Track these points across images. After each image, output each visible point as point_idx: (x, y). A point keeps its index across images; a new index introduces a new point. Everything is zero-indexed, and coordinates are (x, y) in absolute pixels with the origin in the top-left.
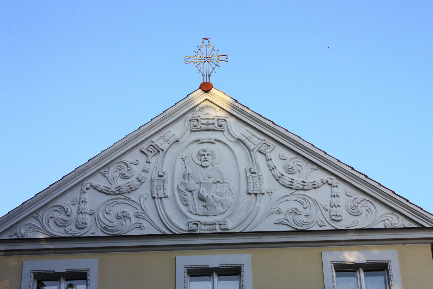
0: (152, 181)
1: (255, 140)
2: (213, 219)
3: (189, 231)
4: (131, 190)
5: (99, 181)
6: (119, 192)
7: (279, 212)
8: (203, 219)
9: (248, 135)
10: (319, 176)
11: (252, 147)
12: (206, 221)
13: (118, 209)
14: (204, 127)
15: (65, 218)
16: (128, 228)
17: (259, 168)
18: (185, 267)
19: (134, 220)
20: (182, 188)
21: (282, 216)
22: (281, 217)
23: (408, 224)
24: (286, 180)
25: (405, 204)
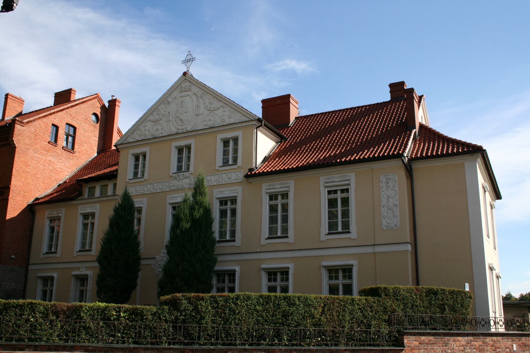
4: (160, 119)
5: (151, 118)
6: (157, 121)
10: (220, 104)
16: (158, 134)
18: (222, 140)
19: (160, 131)
21: (205, 123)
22: (205, 123)
23: (247, 119)
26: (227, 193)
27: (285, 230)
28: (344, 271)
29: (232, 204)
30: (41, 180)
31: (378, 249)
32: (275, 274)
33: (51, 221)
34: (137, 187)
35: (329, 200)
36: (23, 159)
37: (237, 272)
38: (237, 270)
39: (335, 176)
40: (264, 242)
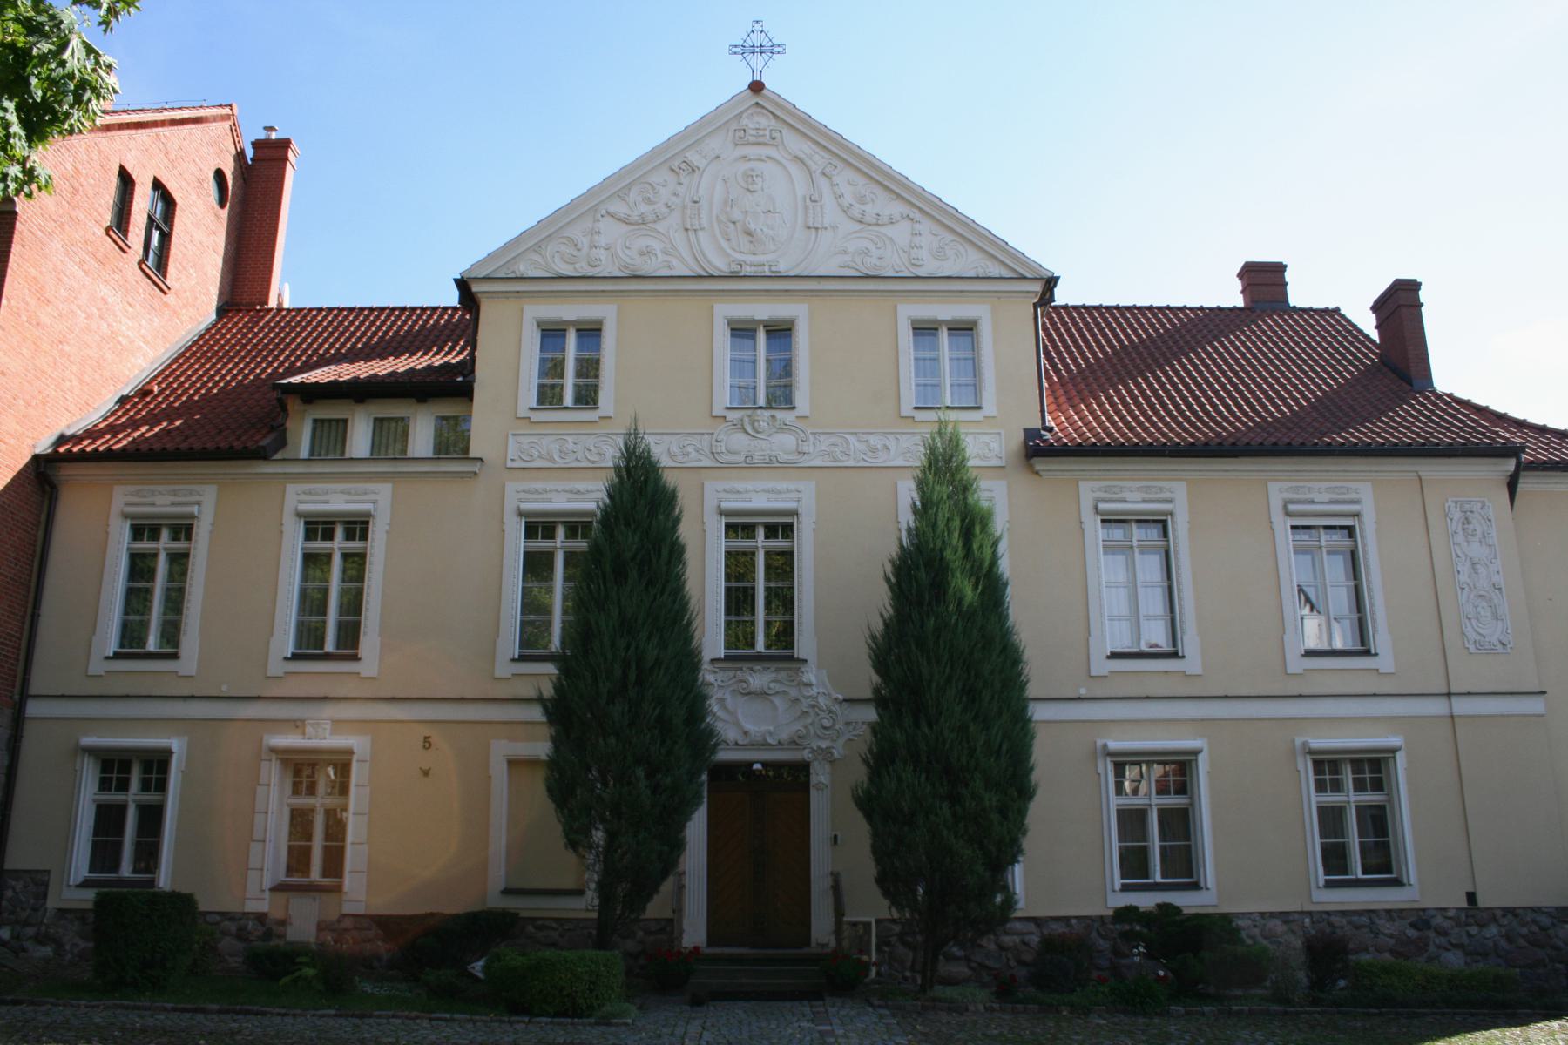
0: (684, 207)
1: (819, 160)
2: (760, 258)
3: (264, 1014)
4: (658, 219)
7: (845, 252)
8: (749, 258)
9: (808, 151)
10: (897, 208)
11: (814, 167)
12: (751, 260)
13: (642, 242)
14: (752, 139)
15: (572, 251)
17: (821, 195)
19: (661, 257)
20: (723, 218)
21: (847, 258)
22: (847, 258)
23: (1005, 273)
24: (856, 212)
25: (1002, 246)
26: (758, 497)
27: (172, 633)
28: (147, 767)
29: (350, 536)
30: (74, 369)
31: (1462, 707)
32: (125, 766)
33: (137, 532)
34: (569, 439)
35: (526, 554)
36: (33, 271)
37: (175, 758)
38: (175, 748)
39: (160, 488)
40: (97, 666)
